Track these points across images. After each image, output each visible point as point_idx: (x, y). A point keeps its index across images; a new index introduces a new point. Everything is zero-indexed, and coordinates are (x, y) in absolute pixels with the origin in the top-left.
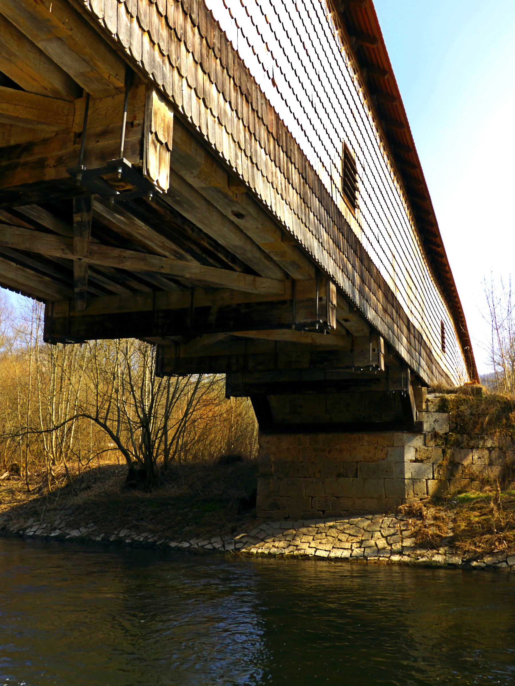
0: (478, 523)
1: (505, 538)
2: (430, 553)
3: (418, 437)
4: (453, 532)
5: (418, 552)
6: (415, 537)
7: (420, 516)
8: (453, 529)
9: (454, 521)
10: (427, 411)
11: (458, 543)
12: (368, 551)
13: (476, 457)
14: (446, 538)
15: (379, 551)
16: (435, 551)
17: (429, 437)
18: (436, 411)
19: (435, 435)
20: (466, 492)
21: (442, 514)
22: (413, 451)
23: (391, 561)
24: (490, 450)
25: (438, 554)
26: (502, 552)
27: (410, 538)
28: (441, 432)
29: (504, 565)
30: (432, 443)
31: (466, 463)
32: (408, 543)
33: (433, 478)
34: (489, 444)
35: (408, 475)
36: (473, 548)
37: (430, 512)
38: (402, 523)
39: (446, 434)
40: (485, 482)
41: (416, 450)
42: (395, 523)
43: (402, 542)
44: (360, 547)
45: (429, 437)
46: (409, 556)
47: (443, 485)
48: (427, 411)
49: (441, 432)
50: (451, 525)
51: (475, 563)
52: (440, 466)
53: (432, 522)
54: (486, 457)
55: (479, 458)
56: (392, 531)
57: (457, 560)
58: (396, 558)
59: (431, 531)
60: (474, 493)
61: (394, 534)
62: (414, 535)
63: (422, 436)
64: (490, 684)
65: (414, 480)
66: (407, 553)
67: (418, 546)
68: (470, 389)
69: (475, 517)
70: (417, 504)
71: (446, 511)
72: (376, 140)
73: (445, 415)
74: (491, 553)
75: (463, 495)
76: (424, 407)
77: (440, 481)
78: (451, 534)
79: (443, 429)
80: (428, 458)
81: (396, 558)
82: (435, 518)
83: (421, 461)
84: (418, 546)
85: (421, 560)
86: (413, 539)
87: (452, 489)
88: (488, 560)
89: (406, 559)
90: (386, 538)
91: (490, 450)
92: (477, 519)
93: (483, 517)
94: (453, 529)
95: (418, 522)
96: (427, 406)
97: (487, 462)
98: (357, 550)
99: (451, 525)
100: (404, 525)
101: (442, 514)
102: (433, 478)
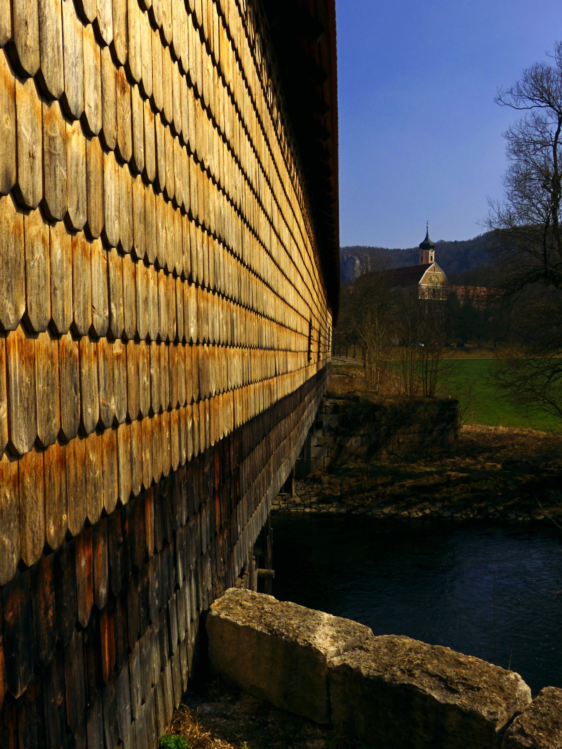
0: (355, 486)
1: (370, 497)
2: (328, 506)
3: (320, 431)
4: (341, 492)
5: (321, 506)
6: (318, 496)
7: (321, 482)
8: (340, 490)
9: (341, 485)
10: (326, 413)
11: (344, 500)
12: (290, 505)
13: (353, 441)
14: (337, 496)
15: (297, 505)
16: (330, 505)
17: (326, 430)
18: (331, 413)
19: (330, 429)
20: (347, 463)
21: (334, 480)
22: (316, 440)
23: (305, 512)
24: (362, 436)
25: (332, 507)
26: (369, 505)
27: (315, 497)
28: (333, 427)
29: (370, 513)
30: (328, 434)
31: (348, 445)
32: (314, 499)
33: (328, 456)
34: (362, 432)
35: (313, 455)
36: (352, 502)
37: (325, 479)
38: (309, 486)
39: (337, 428)
40: (358, 456)
41: (318, 439)
42: (305, 487)
43: (310, 499)
44: (285, 503)
45: (326, 430)
46: (315, 508)
47: (334, 461)
48: (326, 413)
49: (333, 427)
50: (339, 488)
51: (354, 512)
52: (332, 449)
53: (327, 486)
54: (359, 441)
55: (356, 441)
56: (303, 492)
57: (343, 510)
58: (307, 510)
59: (327, 492)
60: (352, 465)
61: (305, 494)
62: (317, 495)
63: (322, 430)
64: (237, 574)
65: (316, 458)
66: (314, 507)
67: (319, 502)
68: (352, 397)
69: (353, 482)
70: (318, 473)
71: (335, 478)
72: (306, 248)
73: (337, 416)
74: (363, 506)
75: (344, 466)
76: (324, 411)
77: (332, 458)
78: (339, 494)
79: (334, 425)
80: (325, 444)
81: (307, 510)
82: (329, 483)
83: (321, 446)
84: (319, 502)
85: (323, 511)
86: (317, 498)
87: (339, 462)
88: (361, 510)
89: (314, 510)
90: (300, 496)
91: (362, 436)
92: (354, 484)
93: (358, 483)
94: (340, 490)
95: (319, 486)
96: (326, 410)
97: (360, 444)
98: (283, 505)
99: (339, 488)
100: (310, 488)
101: (334, 480)
102: (328, 456)
